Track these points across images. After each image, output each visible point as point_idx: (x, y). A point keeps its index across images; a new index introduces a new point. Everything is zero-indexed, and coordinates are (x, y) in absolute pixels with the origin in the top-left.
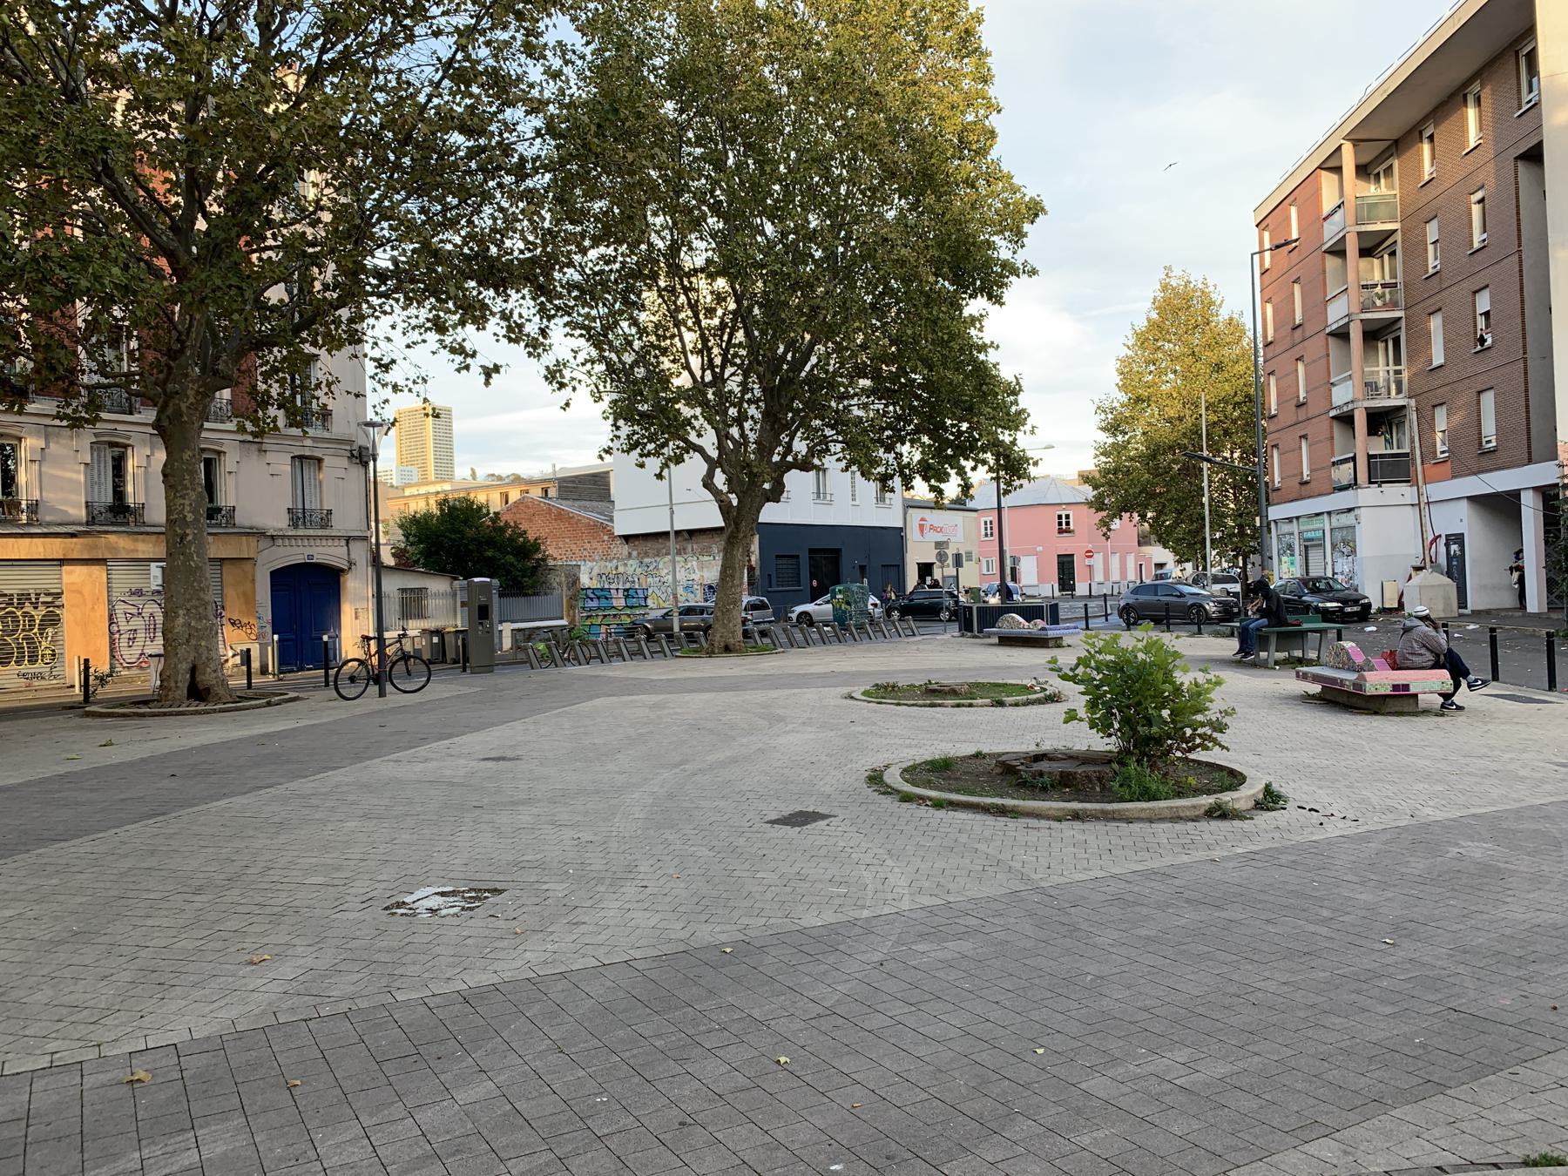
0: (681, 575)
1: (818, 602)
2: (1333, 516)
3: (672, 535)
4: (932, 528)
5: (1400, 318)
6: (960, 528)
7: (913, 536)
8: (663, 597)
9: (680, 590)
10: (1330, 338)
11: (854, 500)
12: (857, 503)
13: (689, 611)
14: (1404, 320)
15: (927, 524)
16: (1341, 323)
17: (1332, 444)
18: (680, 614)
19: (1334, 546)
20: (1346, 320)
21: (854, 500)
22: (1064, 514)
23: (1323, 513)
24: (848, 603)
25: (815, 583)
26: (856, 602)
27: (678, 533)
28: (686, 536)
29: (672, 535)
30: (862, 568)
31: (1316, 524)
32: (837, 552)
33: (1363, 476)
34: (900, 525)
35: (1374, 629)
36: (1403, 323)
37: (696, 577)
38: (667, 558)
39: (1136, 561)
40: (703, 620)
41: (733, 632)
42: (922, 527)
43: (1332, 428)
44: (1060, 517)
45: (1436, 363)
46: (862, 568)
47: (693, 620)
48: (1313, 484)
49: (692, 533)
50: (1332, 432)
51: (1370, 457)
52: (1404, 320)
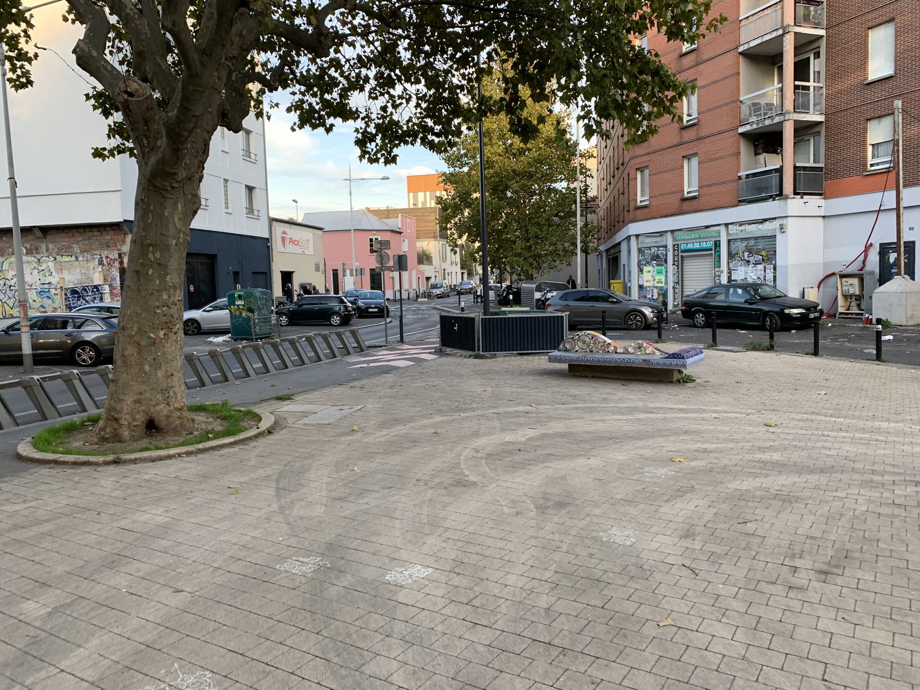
0: (32, 277)
1: (207, 308)
2: (640, 238)
3: (16, 234)
4: (292, 241)
5: (822, 37)
6: (311, 242)
7: (277, 247)
8: (11, 303)
9: (32, 295)
10: (741, 59)
11: (227, 208)
12: (230, 211)
13: (45, 323)
14: (825, 39)
15: (288, 237)
16: (774, 34)
17: (739, 160)
18: (32, 327)
19: (731, 256)
20: (780, 32)
21: (227, 208)
22: (374, 237)
23: (666, 232)
24: (251, 310)
25: (192, 288)
26: (259, 309)
27: (26, 231)
28: (38, 233)
29: (16, 234)
30: (236, 274)
31: (661, 241)
32: (212, 258)
33: (788, 187)
34: (266, 235)
35: (891, 337)
36: (823, 44)
37: (54, 279)
38: (13, 259)
39: (417, 274)
40: (69, 335)
41: (165, 391)
42: (283, 239)
43: (739, 143)
44: (371, 240)
45: (873, 75)
46: (236, 274)
47: (53, 336)
48: (702, 200)
49: (46, 231)
50: (739, 148)
51: (796, 168)
52: (825, 39)
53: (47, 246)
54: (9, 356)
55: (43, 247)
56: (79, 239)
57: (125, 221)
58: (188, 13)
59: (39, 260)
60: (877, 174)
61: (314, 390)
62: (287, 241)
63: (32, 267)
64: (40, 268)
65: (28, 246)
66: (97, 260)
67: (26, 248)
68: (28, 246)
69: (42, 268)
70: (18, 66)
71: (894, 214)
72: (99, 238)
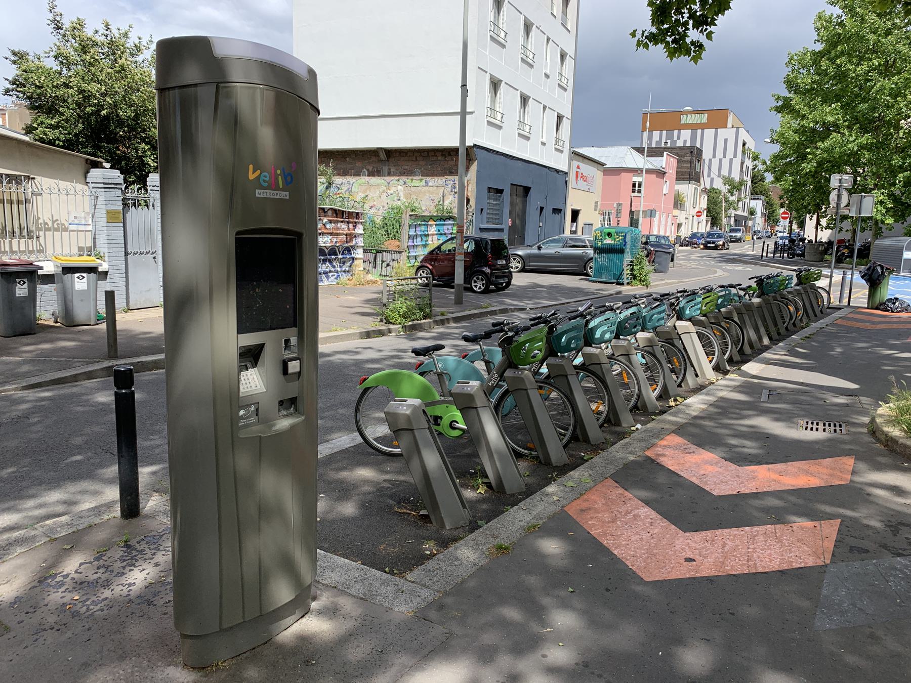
4: (583, 177)
53: (390, 169)
54: (552, 270)
55: (386, 169)
56: (422, 163)
57: (475, 146)
58: (688, 7)
59: (389, 183)
60: (560, 226)
61: (816, 520)
62: (580, 175)
63: (381, 190)
64: (390, 192)
65: (371, 169)
66: (450, 186)
67: (368, 170)
68: (371, 169)
69: (392, 191)
70: (694, 54)
71: (458, 118)
72: (442, 163)
